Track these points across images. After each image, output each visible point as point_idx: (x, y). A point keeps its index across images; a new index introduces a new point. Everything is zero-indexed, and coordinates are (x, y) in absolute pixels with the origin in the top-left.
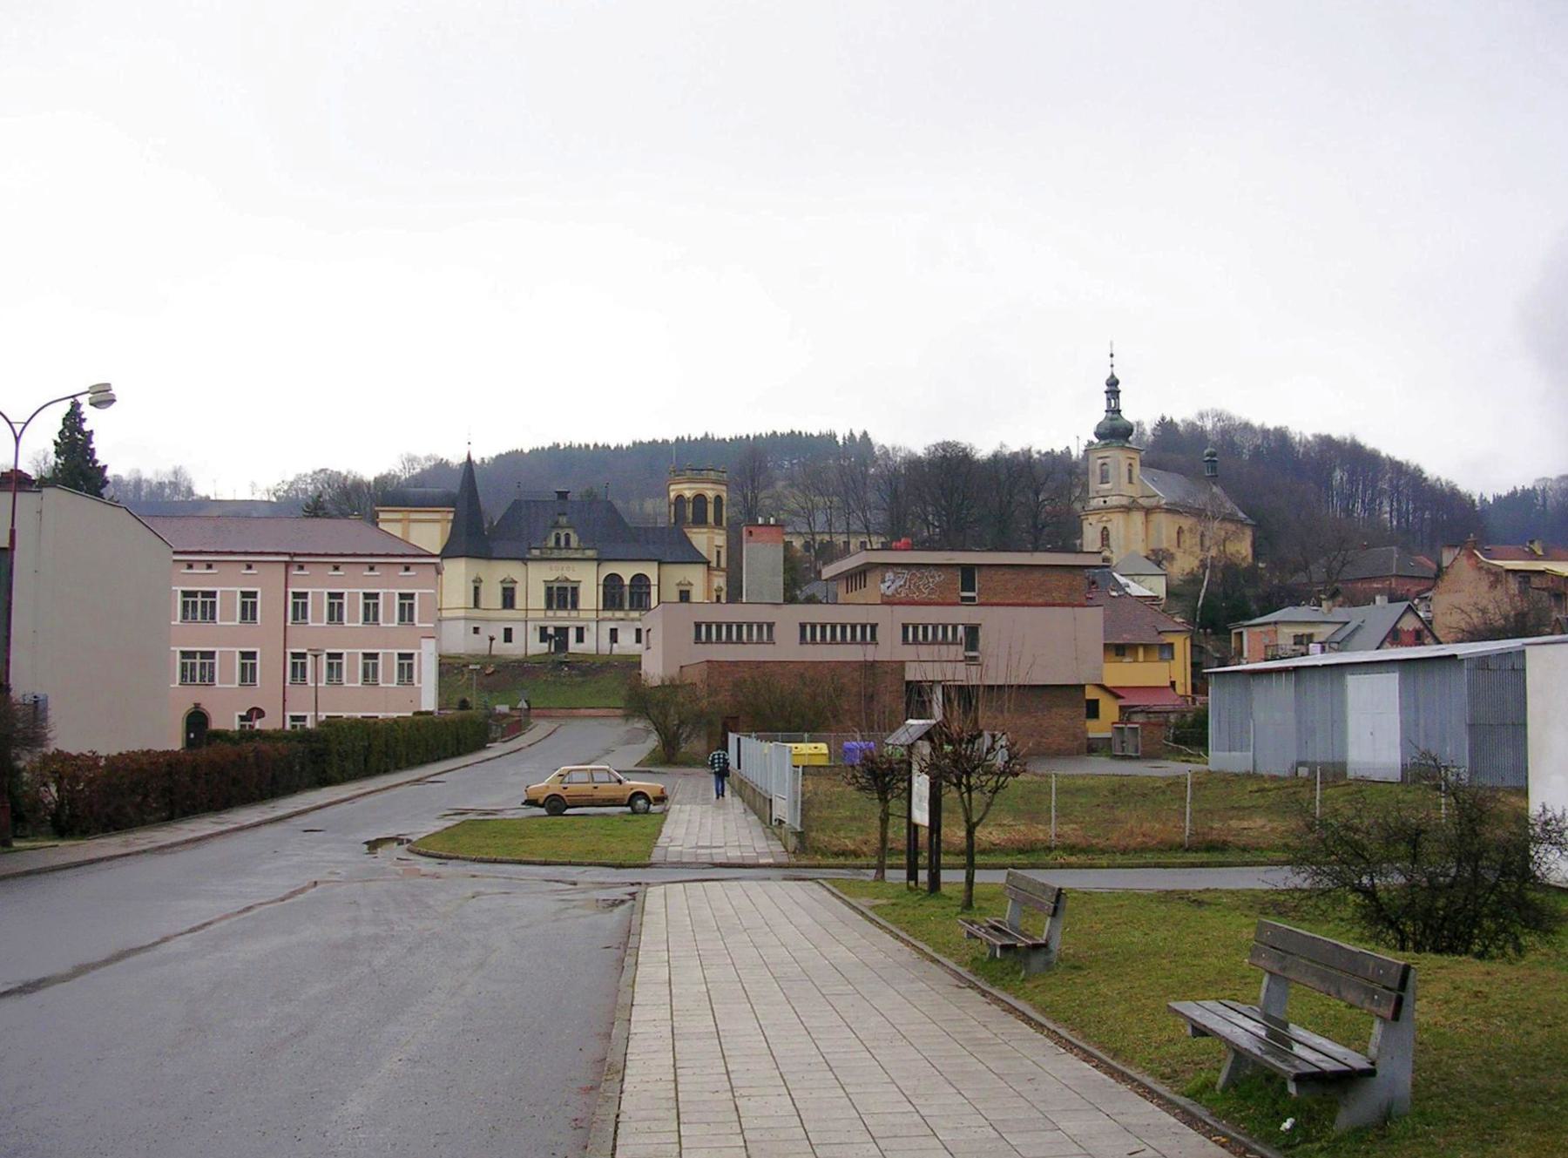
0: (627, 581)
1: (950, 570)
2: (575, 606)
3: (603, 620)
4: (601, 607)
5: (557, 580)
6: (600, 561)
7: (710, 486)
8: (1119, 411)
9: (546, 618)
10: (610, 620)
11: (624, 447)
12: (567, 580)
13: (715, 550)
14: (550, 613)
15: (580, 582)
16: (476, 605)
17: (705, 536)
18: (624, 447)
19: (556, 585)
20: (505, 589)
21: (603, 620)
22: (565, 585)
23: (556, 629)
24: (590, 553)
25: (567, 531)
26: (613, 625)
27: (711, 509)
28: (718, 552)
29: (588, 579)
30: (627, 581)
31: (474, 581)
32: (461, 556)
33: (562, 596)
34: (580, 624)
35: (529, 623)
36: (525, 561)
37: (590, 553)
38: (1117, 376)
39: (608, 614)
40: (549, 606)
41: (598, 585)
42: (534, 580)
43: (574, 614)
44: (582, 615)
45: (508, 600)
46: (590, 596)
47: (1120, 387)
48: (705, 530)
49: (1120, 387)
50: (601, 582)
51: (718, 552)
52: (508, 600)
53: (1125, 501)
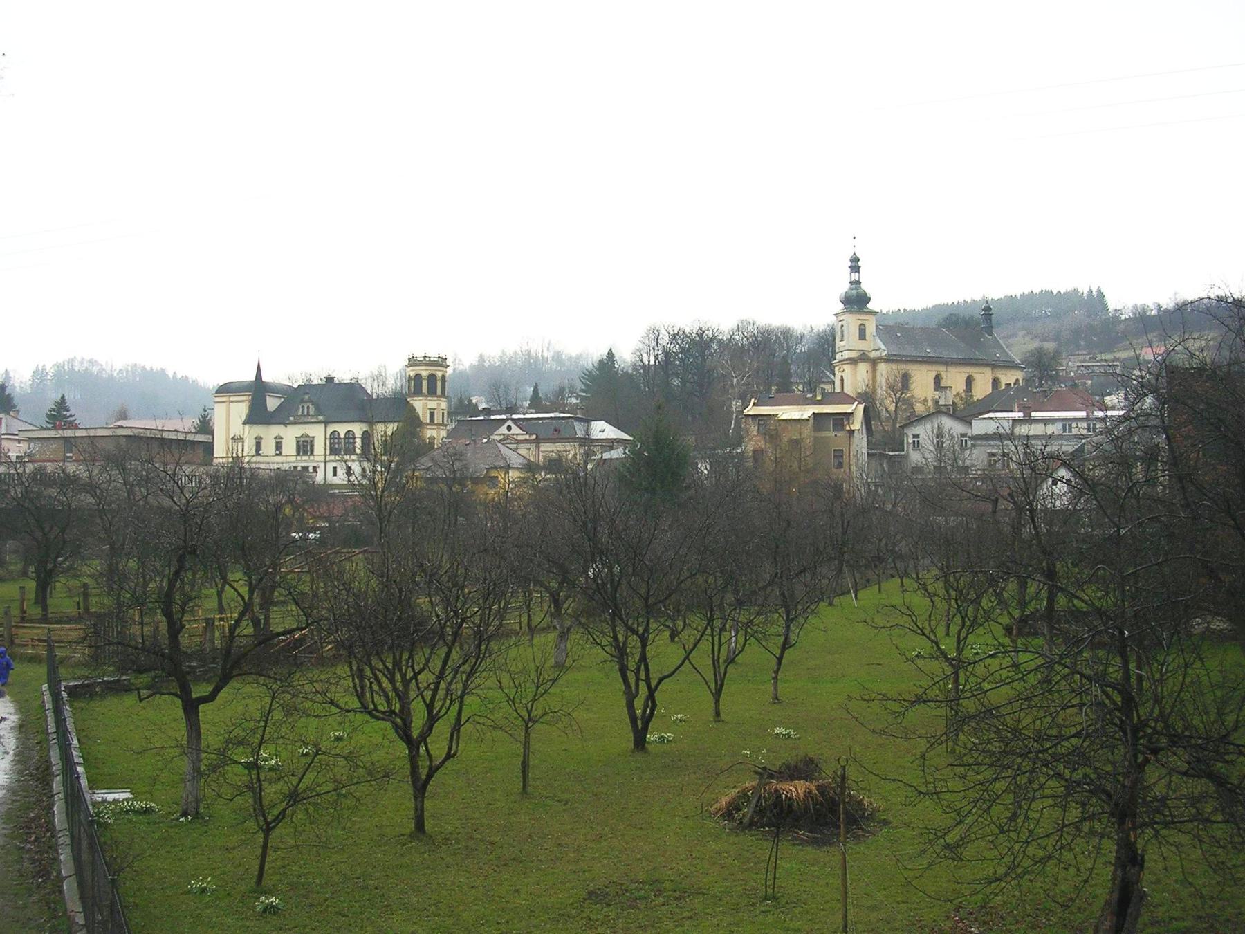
0: (342, 436)
1: (43, 441)
2: (312, 453)
3: (329, 461)
4: (328, 452)
5: (302, 436)
6: (326, 423)
7: (423, 368)
8: (859, 283)
9: (297, 461)
10: (333, 461)
11: (1018, 296)
12: (308, 436)
13: (441, 411)
14: (299, 458)
15: (314, 437)
16: (258, 454)
17: (435, 402)
18: (1018, 296)
19: (302, 439)
20: (277, 443)
21: (329, 461)
22: (307, 439)
23: (303, 467)
24: (321, 418)
25: (308, 404)
26: (334, 464)
27: (425, 383)
28: (443, 413)
29: (318, 433)
30: (342, 436)
31: (256, 438)
32: (356, 421)
33: (305, 446)
34: (315, 464)
35: (328, 464)
36: (285, 424)
37: (321, 418)
38: (858, 255)
39: (332, 458)
40: (298, 454)
41: (326, 438)
42: (290, 435)
43: (312, 457)
44: (317, 458)
45: (278, 446)
46: (319, 447)
47: (860, 263)
48: (421, 398)
49: (860, 263)
50: (328, 436)
51: (443, 413)
52: (278, 446)
53: (854, 355)
